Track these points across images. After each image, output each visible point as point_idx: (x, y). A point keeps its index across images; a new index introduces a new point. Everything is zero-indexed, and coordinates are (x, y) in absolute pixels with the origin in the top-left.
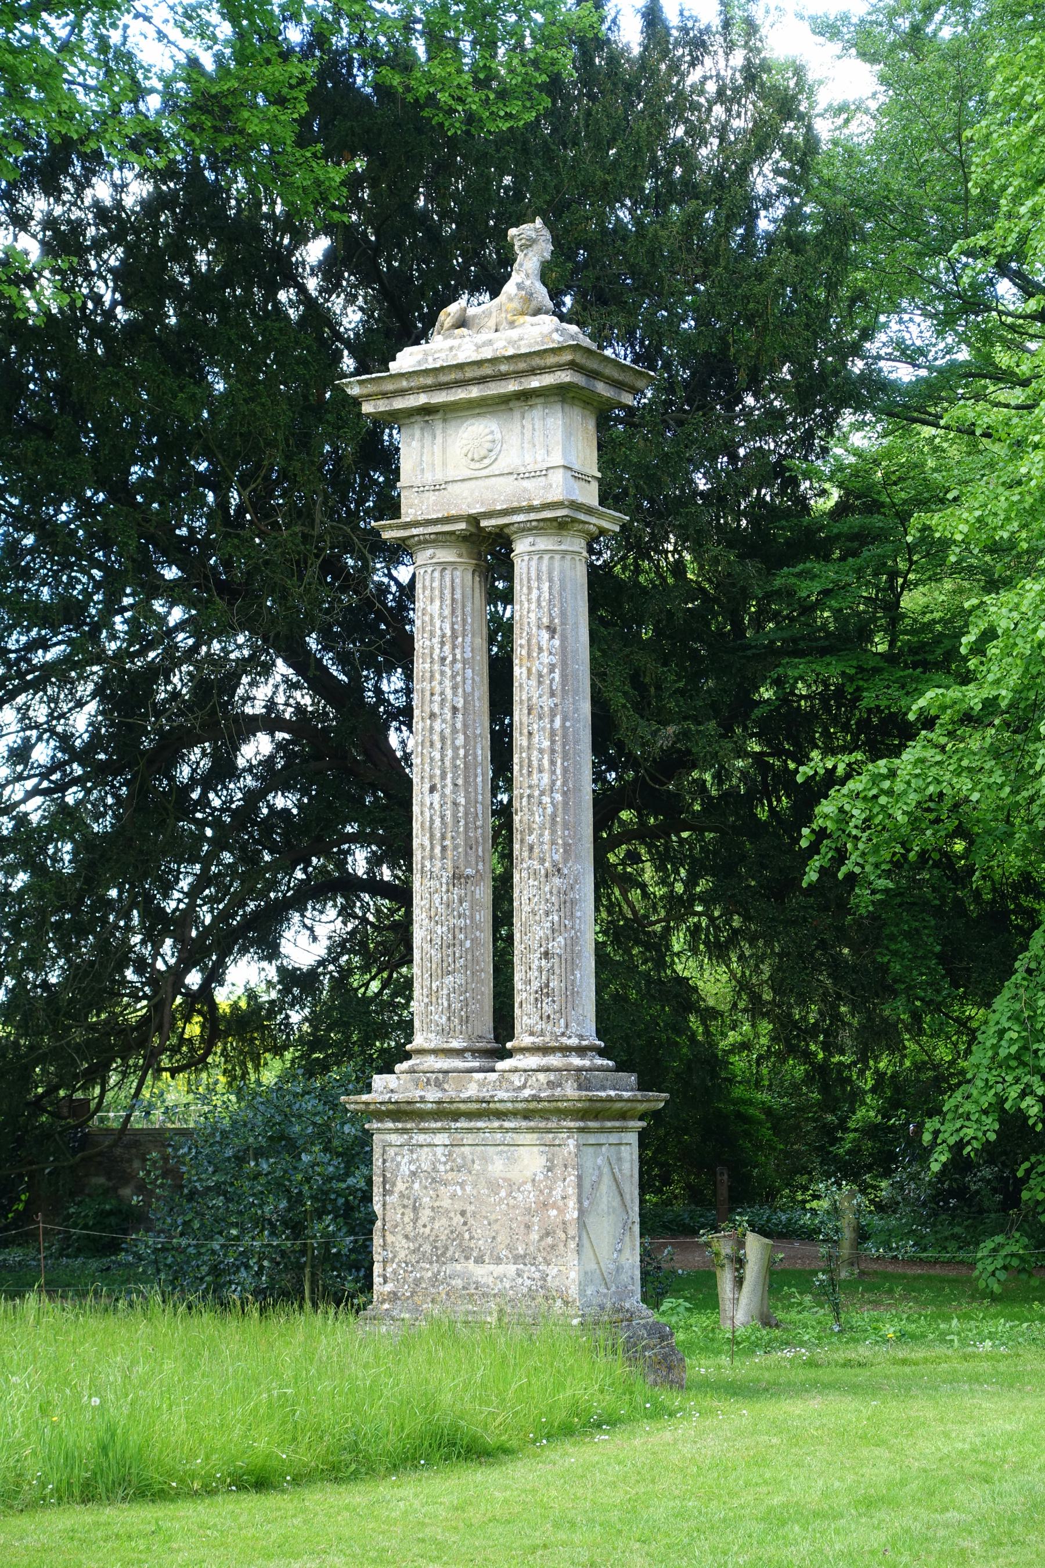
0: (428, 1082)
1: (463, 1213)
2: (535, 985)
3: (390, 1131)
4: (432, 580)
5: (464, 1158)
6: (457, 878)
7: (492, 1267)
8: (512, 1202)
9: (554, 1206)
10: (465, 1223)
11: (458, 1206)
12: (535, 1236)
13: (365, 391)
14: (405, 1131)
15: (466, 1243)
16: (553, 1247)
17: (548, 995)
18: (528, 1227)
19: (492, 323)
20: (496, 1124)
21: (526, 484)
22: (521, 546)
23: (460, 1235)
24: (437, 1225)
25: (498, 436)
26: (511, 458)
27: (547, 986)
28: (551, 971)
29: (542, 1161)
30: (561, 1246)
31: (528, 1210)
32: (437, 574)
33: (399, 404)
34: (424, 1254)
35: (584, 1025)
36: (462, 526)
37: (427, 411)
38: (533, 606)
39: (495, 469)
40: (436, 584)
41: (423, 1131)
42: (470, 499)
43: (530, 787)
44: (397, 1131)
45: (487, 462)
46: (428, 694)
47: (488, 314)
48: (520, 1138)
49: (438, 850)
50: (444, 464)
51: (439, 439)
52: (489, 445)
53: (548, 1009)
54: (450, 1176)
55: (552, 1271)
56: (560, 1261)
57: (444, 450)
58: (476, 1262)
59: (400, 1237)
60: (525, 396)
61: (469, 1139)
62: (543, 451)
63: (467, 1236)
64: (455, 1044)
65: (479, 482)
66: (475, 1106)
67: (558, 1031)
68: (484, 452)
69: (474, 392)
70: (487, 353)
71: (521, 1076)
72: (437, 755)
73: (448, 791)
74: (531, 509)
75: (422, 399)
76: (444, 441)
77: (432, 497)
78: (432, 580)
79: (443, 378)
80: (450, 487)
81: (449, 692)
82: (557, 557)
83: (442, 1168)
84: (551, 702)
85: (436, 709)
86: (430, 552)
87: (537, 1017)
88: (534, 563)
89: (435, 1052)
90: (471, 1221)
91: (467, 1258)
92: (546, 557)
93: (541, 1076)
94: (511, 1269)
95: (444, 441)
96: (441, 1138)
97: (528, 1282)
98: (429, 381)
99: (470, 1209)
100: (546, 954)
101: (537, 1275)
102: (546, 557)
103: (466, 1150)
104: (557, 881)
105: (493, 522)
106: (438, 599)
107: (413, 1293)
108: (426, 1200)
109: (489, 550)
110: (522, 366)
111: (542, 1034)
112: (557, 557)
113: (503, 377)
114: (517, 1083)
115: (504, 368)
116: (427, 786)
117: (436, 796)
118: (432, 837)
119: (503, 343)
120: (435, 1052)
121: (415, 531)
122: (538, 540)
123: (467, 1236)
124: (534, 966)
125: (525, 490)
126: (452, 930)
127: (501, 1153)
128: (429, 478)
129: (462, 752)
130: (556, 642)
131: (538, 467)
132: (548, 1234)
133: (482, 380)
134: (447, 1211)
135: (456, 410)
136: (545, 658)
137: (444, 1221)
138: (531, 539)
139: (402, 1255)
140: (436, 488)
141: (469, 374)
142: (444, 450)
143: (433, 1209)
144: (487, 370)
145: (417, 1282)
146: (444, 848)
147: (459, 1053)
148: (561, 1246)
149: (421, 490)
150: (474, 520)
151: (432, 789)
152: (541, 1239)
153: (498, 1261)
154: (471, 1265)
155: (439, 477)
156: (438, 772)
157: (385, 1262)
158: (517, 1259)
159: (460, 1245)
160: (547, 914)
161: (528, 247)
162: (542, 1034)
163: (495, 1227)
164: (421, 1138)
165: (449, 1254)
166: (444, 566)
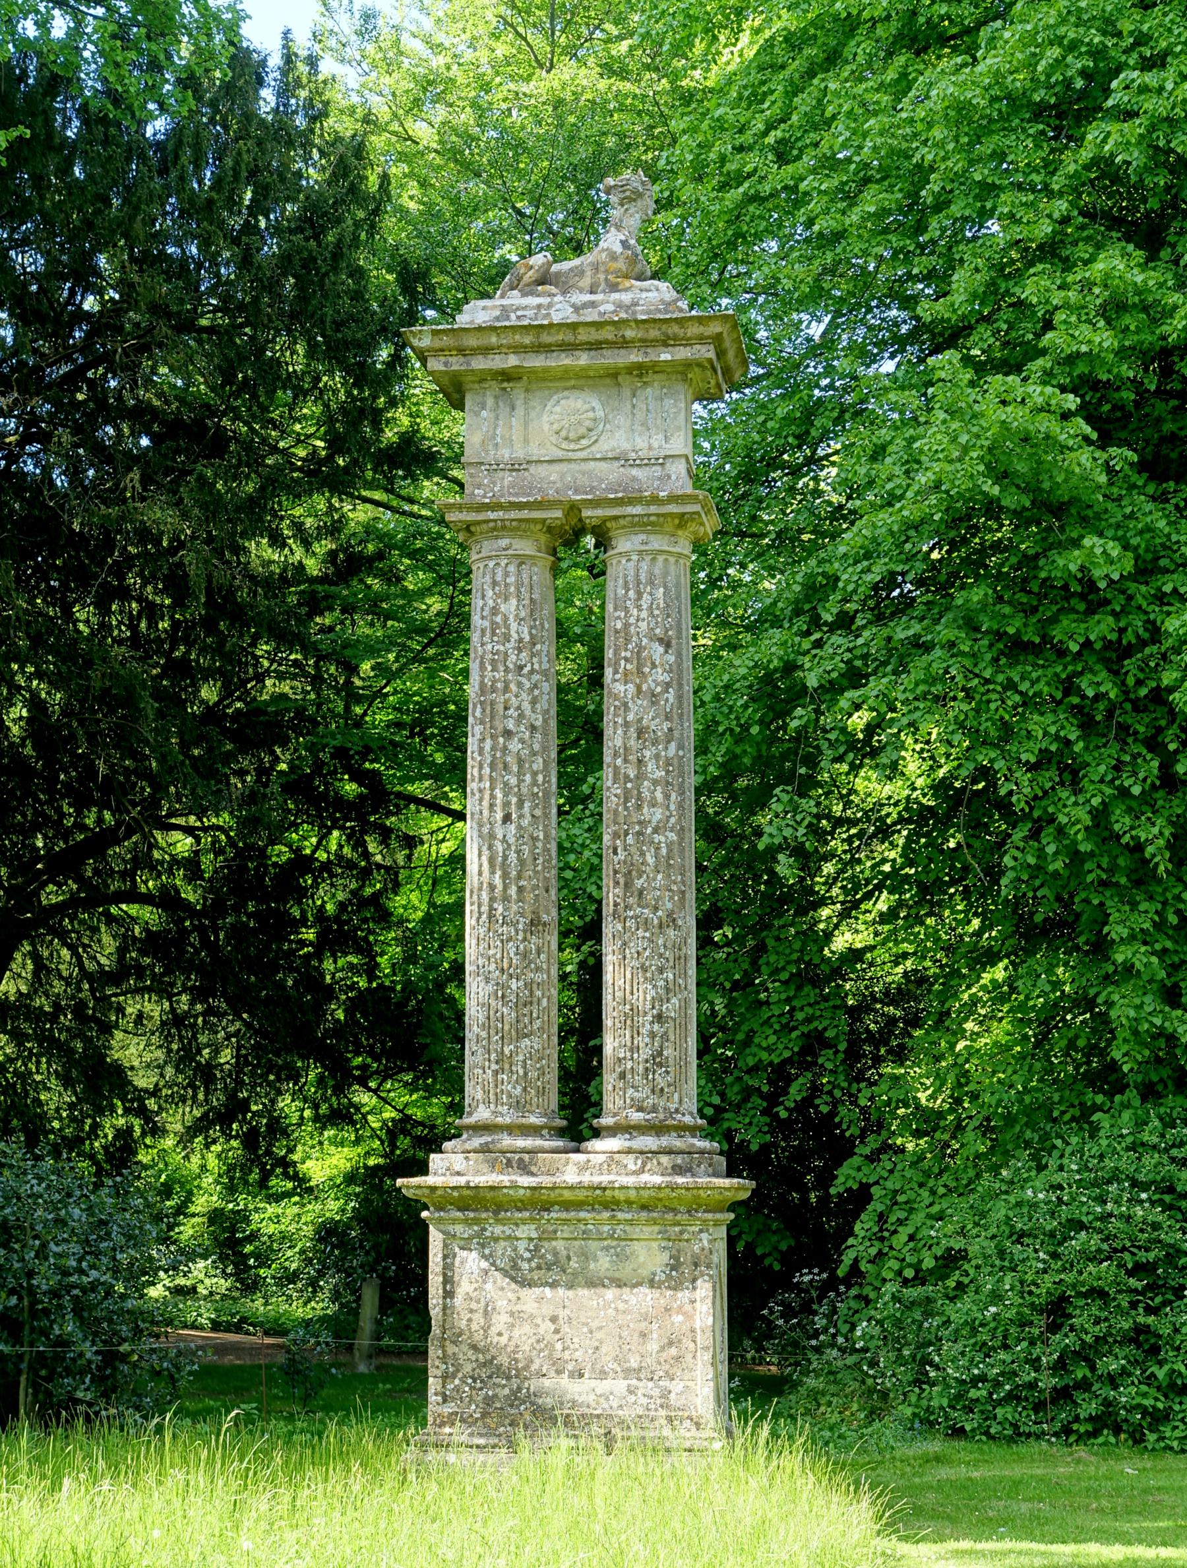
0: (509, 1163)
1: (554, 1319)
2: (645, 1053)
3: (454, 1221)
4: (506, 574)
5: (556, 1254)
6: (535, 924)
7: (593, 1383)
8: (621, 1306)
9: (680, 1310)
10: (557, 1331)
11: (548, 1310)
12: (653, 1346)
13: (438, 344)
14: (476, 1221)
15: (557, 1355)
16: (678, 1359)
17: (660, 1065)
18: (643, 1335)
19: (586, 282)
20: (606, 1215)
21: (634, 472)
22: (624, 544)
23: (550, 1346)
24: (516, 1333)
25: (600, 414)
26: (617, 440)
27: (660, 1054)
28: (665, 1037)
29: (665, 1257)
30: (689, 1357)
31: (645, 1317)
32: (512, 568)
33: (480, 363)
34: (499, 1367)
35: (686, 1102)
36: (558, 514)
37: (507, 376)
38: (644, 614)
39: (606, 445)
40: (511, 580)
41: (498, 1221)
42: (554, 480)
43: (640, 823)
44: (467, 1222)
45: (584, 442)
46: (500, 708)
47: (579, 272)
48: (635, 1232)
49: (513, 891)
50: (526, 441)
51: (520, 411)
52: (588, 423)
53: (661, 1082)
54: (536, 1275)
55: (676, 1386)
56: (687, 1376)
57: (526, 424)
58: (571, 1375)
59: (465, 1348)
60: (639, 371)
61: (565, 1231)
62: (661, 436)
63: (559, 1346)
64: (533, 1120)
65: (573, 466)
66: (581, 1195)
67: (673, 1107)
68: (582, 431)
69: (583, 359)
70: (591, 316)
71: (602, 1163)
72: (513, 781)
73: (525, 822)
74: (655, 500)
75: (513, 361)
76: (527, 414)
77: (508, 479)
78: (506, 574)
79: (546, 338)
80: (532, 469)
81: (526, 706)
82: (672, 560)
83: (525, 1266)
84: (666, 726)
85: (511, 725)
86: (504, 543)
87: (647, 1090)
88: (644, 566)
89: (510, 1129)
90: (565, 1329)
91: (559, 1372)
92: (661, 558)
93: (665, 1159)
94: (621, 1385)
95: (527, 414)
96: (524, 1231)
97: (645, 1401)
98: (527, 340)
99: (563, 1314)
100: (659, 1018)
101: (656, 1393)
102: (661, 558)
103: (559, 1245)
104: (671, 933)
105: (599, 512)
106: (506, 603)
107: (485, 1415)
108: (501, 1304)
109: (576, 539)
110: (654, 333)
111: (654, 1109)
112: (672, 560)
113: (624, 344)
114: (632, 1167)
115: (629, 334)
116: (499, 816)
117: (513, 828)
118: (505, 876)
119: (610, 307)
120: (510, 1129)
121: (491, 515)
122: (652, 537)
123: (559, 1346)
124: (644, 1031)
125: (634, 479)
126: (529, 985)
127: (607, 1248)
128: (505, 454)
129: (540, 778)
130: (671, 658)
131: (652, 454)
132: (671, 1344)
133: (595, 346)
134: (532, 1317)
135: (544, 380)
136: (661, 676)
137: (527, 1328)
138: (643, 537)
139: (468, 1368)
140: (515, 467)
141: (583, 336)
142: (526, 424)
143: (512, 1314)
144: (608, 334)
145: (489, 1401)
146: (520, 889)
147: (535, 1131)
148: (689, 1357)
149: (495, 468)
150: (573, 508)
151: (507, 818)
152: (662, 1349)
153: (603, 1375)
154: (564, 1380)
155: (520, 454)
156: (514, 800)
157: (445, 1377)
158: (628, 1373)
159: (550, 1357)
160: (661, 970)
161: (631, 200)
162: (654, 1109)
163: (599, 1335)
164: (498, 1230)
165: (534, 1367)
166: (521, 560)
